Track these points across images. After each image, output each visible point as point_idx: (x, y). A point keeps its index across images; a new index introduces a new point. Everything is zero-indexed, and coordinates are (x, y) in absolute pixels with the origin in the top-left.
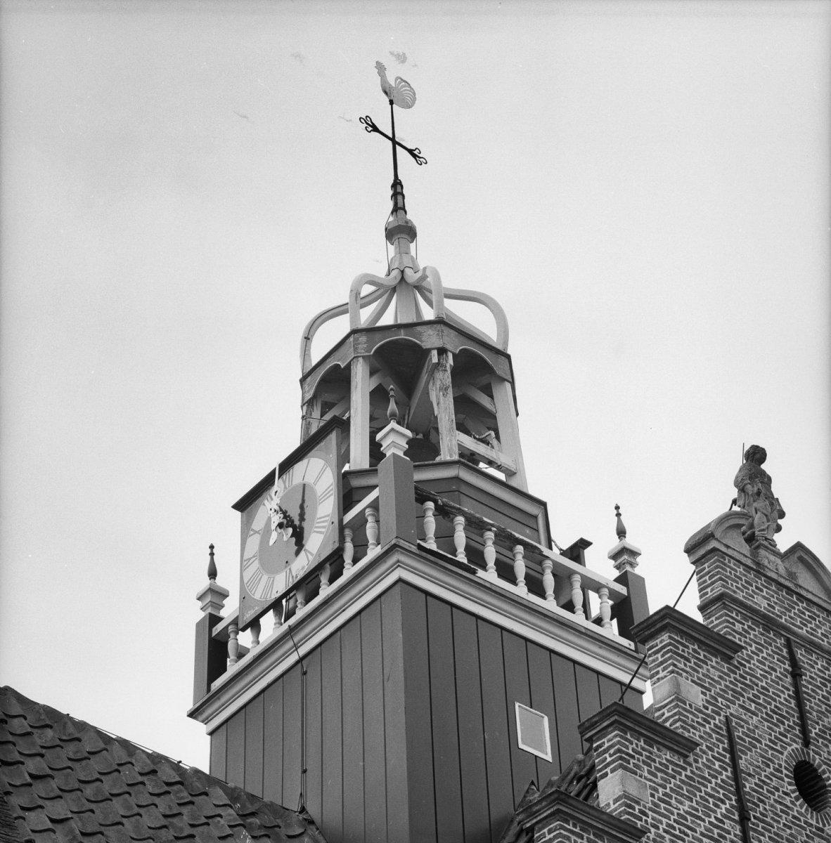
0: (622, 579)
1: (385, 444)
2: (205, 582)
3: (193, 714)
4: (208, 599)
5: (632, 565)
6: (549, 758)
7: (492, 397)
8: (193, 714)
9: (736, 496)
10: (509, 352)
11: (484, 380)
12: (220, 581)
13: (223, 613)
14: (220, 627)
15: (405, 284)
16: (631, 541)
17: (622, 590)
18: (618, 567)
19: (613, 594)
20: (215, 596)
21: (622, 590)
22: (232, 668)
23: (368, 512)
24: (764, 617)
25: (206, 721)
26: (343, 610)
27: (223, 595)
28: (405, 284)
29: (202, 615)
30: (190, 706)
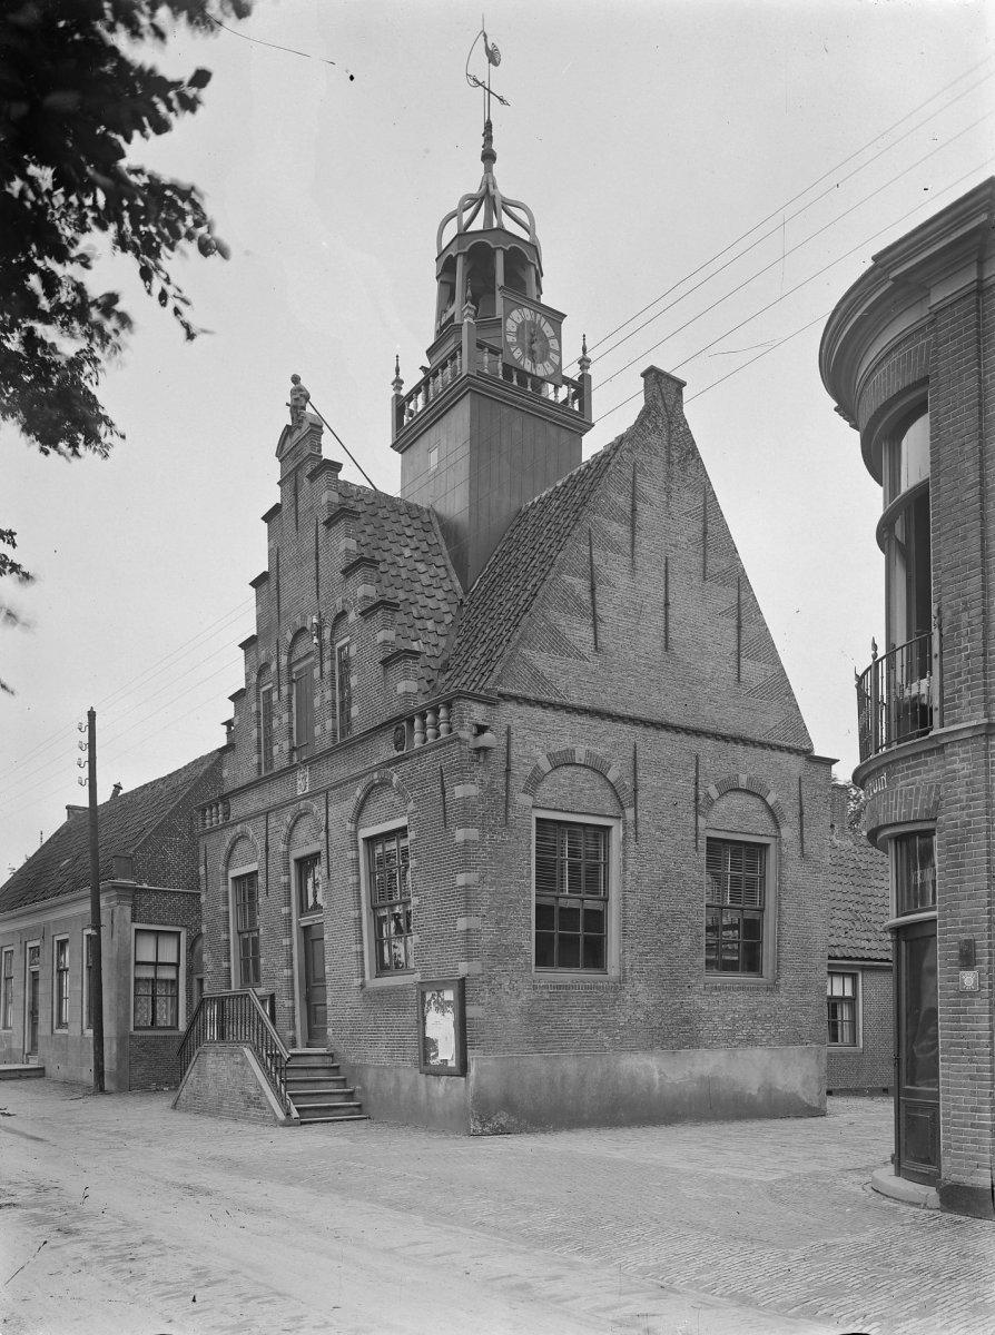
0: (581, 378)
15: (486, 198)
20: (398, 383)
28: (486, 198)
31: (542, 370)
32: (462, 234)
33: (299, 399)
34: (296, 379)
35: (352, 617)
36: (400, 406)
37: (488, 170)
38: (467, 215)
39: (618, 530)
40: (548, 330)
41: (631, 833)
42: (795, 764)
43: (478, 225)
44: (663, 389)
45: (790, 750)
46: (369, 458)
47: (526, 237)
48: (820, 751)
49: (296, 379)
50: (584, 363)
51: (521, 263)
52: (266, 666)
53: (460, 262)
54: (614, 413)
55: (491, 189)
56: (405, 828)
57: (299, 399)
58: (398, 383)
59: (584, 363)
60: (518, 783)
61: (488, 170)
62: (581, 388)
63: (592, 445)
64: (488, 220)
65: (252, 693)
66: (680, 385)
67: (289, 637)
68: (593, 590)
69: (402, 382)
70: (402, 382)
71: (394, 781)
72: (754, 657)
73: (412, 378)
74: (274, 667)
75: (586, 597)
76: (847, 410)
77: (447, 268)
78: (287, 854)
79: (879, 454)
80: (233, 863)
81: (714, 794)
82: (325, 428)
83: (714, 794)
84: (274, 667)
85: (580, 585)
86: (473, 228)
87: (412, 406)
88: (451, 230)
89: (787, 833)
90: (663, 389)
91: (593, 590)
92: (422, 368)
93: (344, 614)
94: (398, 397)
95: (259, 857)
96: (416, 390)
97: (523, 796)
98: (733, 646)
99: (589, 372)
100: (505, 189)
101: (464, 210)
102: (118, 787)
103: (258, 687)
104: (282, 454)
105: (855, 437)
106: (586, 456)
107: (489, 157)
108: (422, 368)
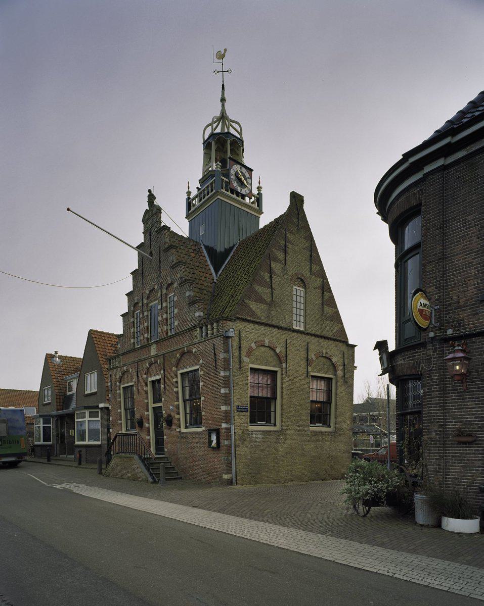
0: (258, 194)
15: (223, 117)
16: (261, 185)
19: (257, 197)
20: (189, 193)
22: (193, 208)
25: (188, 219)
28: (223, 117)
31: (244, 191)
32: (212, 135)
33: (151, 198)
34: (150, 191)
35: (175, 285)
36: (189, 205)
37: (223, 106)
38: (215, 125)
39: (280, 255)
40: (247, 175)
41: (284, 372)
42: (343, 347)
43: (218, 130)
44: (296, 200)
45: (340, 341)
46: (177, 222)
47: (239, 136)
48: (350, 342)
49: (150, 191)
50: (259, 188)
51: (237, 144)
52: (137, 303)
53: (213, 143)
54: (273, 209)
55: (225, 115)
56: (198, 369)
57: (151, 198)
58: (189, 193)
59: (259, 188)
60: (244, 353)
61: (223, 106)
62: (259, 200)
63: (265, 220)
64: (223, 128)
65: (131, 315)
66: (303, 197)
67: (147, 292)
68: (271, 277)
69: (191, 193)
70: (191, 193)
71: (194, 351)
72: (328, 305)
73: (194, 192)
74: (140, 305)
75: (269, 280)
76: (385, 219)
77: (207, 145)
78: (146, 379)
79: (396, 235)
80: (122, 382)
81: (314, 358)
82: (162, 211)
83: (314, 358)
84: (140, 305)
85: (266, 276)
86: (216, 132)
87: (194, 202)
88: (209, 131)
89: (339, 372)
90: (296, 200)
91: (271, 277)
92: (197, 188)
93: (172, 284)
94: (189, 198)
95: (134, 380)
96: (196, 196)
97: (245, 358)
98: (321, 302)
99: (261, 192)
100: (230, 114)
101: (214, 123)
102: (381, 346)
103: (134, 311)
104: (145, 221)
105: (385, 227)
106: (261, 226)
107: (223, 100)
108: (197, 188)
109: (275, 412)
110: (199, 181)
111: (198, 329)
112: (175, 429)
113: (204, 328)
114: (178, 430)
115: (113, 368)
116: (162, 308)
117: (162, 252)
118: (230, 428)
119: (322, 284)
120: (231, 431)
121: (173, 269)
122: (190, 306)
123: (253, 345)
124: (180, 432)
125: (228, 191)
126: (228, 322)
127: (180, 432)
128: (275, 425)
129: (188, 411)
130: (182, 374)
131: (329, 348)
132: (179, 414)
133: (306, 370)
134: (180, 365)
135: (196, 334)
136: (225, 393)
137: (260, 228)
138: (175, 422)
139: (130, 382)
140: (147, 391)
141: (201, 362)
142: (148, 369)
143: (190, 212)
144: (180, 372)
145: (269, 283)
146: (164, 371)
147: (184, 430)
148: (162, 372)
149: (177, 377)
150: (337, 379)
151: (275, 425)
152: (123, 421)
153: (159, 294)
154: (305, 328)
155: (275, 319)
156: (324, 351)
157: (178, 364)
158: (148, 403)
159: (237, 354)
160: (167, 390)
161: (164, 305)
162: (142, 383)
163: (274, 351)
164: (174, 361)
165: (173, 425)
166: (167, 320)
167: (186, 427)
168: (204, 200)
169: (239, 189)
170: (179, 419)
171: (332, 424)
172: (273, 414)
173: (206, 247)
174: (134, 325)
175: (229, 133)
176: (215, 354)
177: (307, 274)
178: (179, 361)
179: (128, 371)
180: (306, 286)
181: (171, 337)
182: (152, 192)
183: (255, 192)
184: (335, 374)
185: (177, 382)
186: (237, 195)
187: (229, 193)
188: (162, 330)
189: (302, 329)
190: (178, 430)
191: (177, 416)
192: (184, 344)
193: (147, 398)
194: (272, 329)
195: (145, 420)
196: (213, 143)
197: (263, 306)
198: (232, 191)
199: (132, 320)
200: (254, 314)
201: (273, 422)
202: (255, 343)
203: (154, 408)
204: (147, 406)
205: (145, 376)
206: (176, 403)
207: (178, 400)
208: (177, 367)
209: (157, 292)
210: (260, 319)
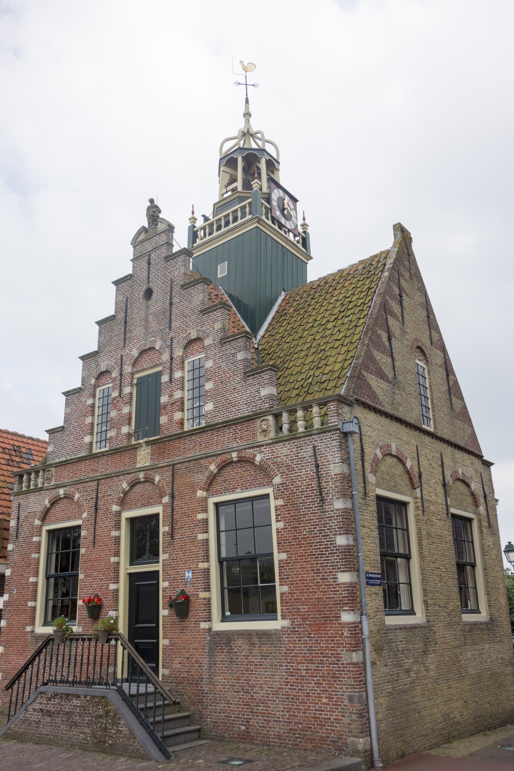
0: (305, 232)
1: (254, 186)
2: (191, 215)
3: (131, 260)
4: (192, 220)
5: (307, 229)
6: (219, 277)
7: (273, 174)
8: (131, 260)
9: (484, 458)
10: (280, 161)
11: (272, 168)
12: (195, 215)
13: (195, 225)
14: (195, 229)
17: (304, 235)
18: (190, 223)
20: (194, 220)
21: (304, 235)
22: (198, 242)
23: (247, 205)
24: (174, 495)
26: (239, 231)
27: (196, 219)
28: (247, 134)
29: (190, 224)
30: (132, 258)
31: (289, 225)
48: (487, 457)
50: (304, 225)
58: (194, 220)
62: (305, 242)
67: (135, 353)
68: (389, 339)
70: (196, 219)
75: (387, 344)
78: (119, 514)
95: (85, 515)
99: (307, 231)
109: (409, 584)
110: (214, 205)
111: (270, 418)
112: (197, 623)
113: (285, 417)
114: (204, 625)
115: (29, 491)
116: (171, 381)
117: (177, 288)
118: (361, 622)
119: (444, 360)
120: (361, 629)
121: (204, 314)
122: (249, 376)
123: (378, 452)
124: (210, 629)
125: (268, 219)
126: (343, 405)
127: (210, 629)
128: (411, 612)
129: (226, 585)
130: (217, 505)
131: (466, 467)
132: (208, 589)
133: (444, 503)
134: (216, 487)
135: (265, 427)
136: (348, 545)
137: (309, 281)
138: (196, 609)
139: (75, 518)
140: (117, 539)
141: (277, 480)
142: (126, 493)
143: (195, 245)
144: (212, 501)
145: (388, 348)
146: (173, 497)
147: (219, 626)
148: (166, 500)
149: (206, 511)
150: (480, 521)
151: (411, 612)
152: (39, 604)
153: (166, 357)
154: (435, 428)
155: (401, 409)
156: (460, 471)
157: (210, 485)
158: (118, 563)
159: (359, 467)
160: (177, 536)
161: (178, 375)
162: (105, 523)
163: (404, 464)
164: (201, 478)
165: (191, 614)
166: (183, 403)
167: (224, 619)
168: (226, 229)
169: (283, 221)
170: (209, 600)
171: (419, 607)
172: (403, 588)
173: (231, 297)
174: (93, 411)
175: (264, 150)
176: (317, 466)
177: (428, 344)
178: (212, 479)
179: (68, 497)
180: (427, 361)
181: (192, 433)
182: (156, 203)
183: (300, 229)
184: (477, 513)
185: (206, 521)
186: (280, 228)
187: (270, 222)
188: (171, 420)
189: (431, 429)
190: (204, 625)
191: (203, 595)
192: (231, 443)
193: (117, 554)
194: (398, 425)
195: (105, 602)
196: (240, 160)
197: (384, 385)
198: (273, 220)
199: (90, 402)
200: (374, 396)
201: (405, 606)
202: (381, 448)
203: (130, 575)
204: (117, 571)
205: (115, 508)
206: (202, 565)
207: (207, 559)
208: (207, 490)
209: (160, 352)
210: (383, 406)
